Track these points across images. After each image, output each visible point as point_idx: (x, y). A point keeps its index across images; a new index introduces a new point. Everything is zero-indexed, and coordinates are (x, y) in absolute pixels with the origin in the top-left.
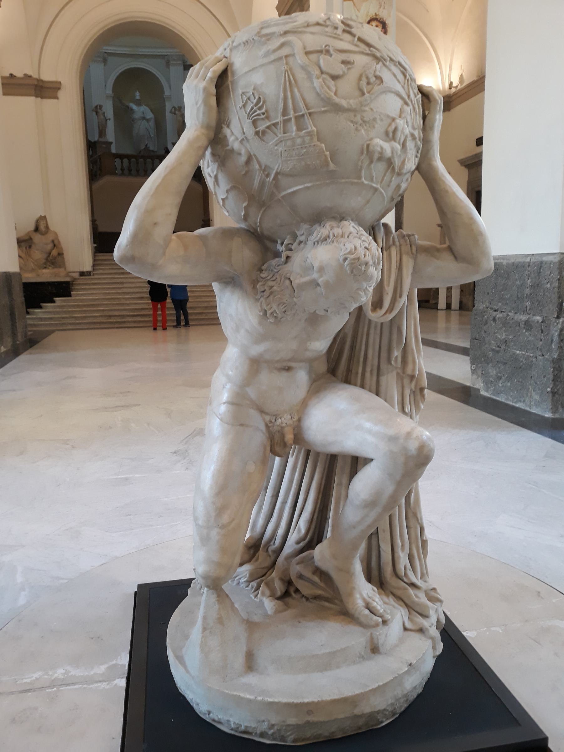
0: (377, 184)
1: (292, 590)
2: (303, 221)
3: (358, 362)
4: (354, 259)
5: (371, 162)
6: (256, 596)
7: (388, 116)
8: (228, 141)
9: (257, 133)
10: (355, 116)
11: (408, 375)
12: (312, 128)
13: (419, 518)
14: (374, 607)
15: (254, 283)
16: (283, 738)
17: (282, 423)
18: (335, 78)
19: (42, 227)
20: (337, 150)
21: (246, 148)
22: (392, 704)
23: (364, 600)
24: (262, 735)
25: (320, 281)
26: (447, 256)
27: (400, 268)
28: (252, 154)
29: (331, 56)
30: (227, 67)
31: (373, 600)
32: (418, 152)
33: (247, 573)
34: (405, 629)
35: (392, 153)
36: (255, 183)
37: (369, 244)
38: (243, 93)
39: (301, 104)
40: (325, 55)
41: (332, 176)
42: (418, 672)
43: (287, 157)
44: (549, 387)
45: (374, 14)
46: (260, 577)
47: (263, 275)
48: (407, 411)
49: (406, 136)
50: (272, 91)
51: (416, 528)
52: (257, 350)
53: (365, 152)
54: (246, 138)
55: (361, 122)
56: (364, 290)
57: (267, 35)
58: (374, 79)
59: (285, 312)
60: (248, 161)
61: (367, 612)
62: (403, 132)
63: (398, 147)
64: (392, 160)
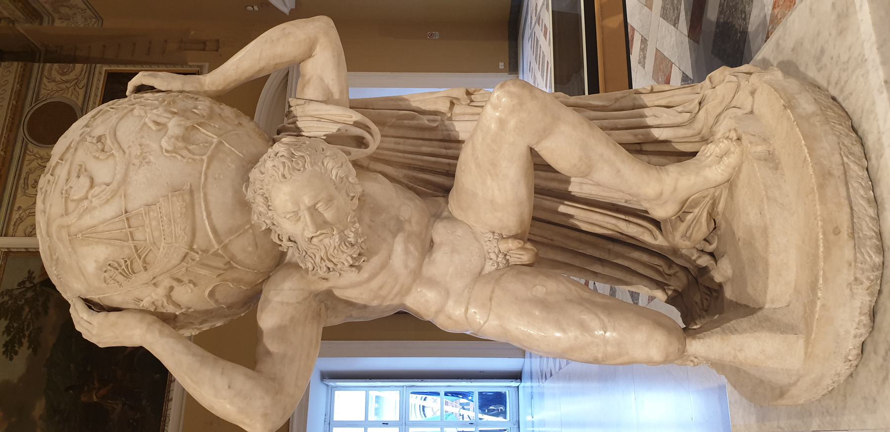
10: (134, 165)
18: (92, 185)
29: (71, 187)
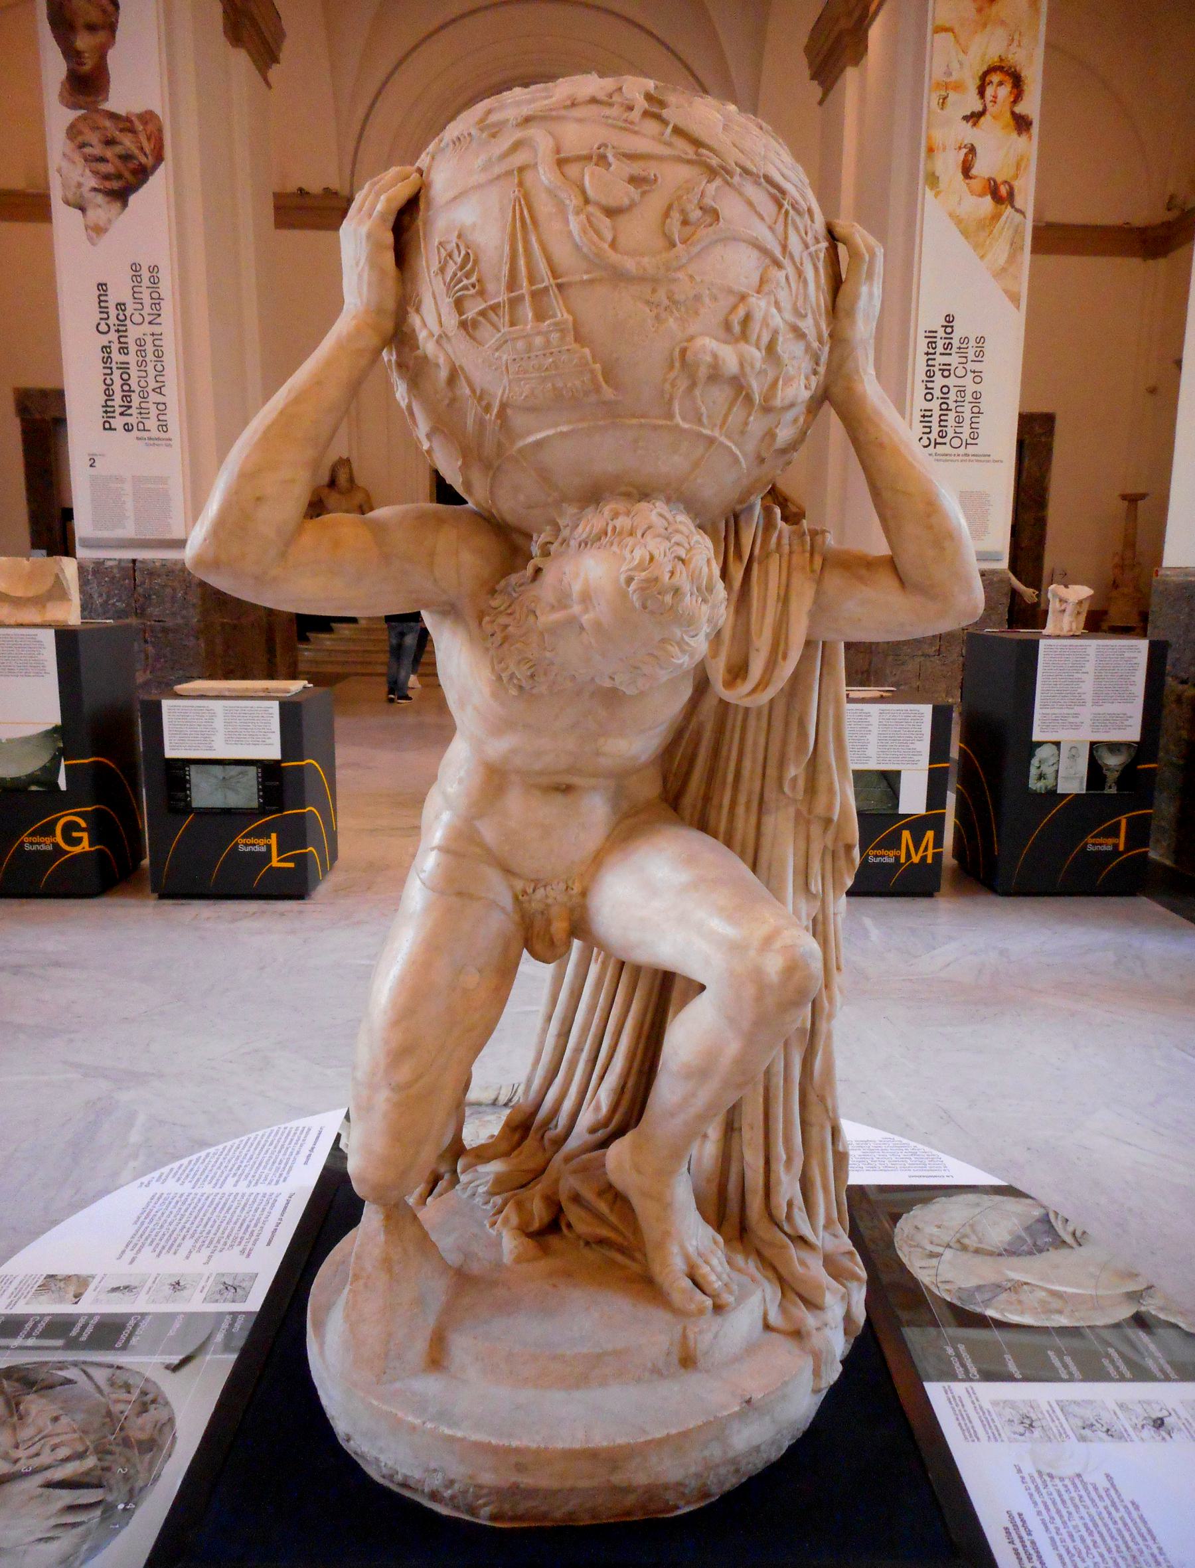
0: (712, 430)
3: (724, 783)
4: (647, 580)
5: (693, 384)
6: (493, 1224)
7: (730, 291)
8: (417, 339)
9: (463, 325)
10: (654, 291)
11: (820, 818)
12: (561, 314)
13: (830, 1107)
14: (704, 1276)
16: (472, 1510)
17: (547, 897)
18: (611, 212)
19: (342, 478)
20: (618, 359)
21: (447, 354)
22: (698, 1475)
23: (687, 1258)
24: (434, 1496)
25: (586, 619)
26: (886, 580)
27: (785, 600)
30: (419, 192)
31: (707, 1262)
32: (817, 364)
33: (491, 1177)
34: (767, 1327)
35: (742, 365)
37: (688, 551)
38: (440, 243)
39: (543, 267)
40: (596, 165)
41: (612, 413)
42: (767, 1418)
43: (518, 373)
45: (996, 59)
46: (511, 1188)
47: (494, 603)
48: (813, 889)
49: (776, 333)
51: (822, 1127)
52: (498, 747)
53: (677, 364)
55: (666, 302)
56: (678, 644)
57: (494, 125)
58: (699, 213)
59: (532, 676)
60: (452, 380)
62: (765, 322)
63: (756, 355)
64: (742, 380)
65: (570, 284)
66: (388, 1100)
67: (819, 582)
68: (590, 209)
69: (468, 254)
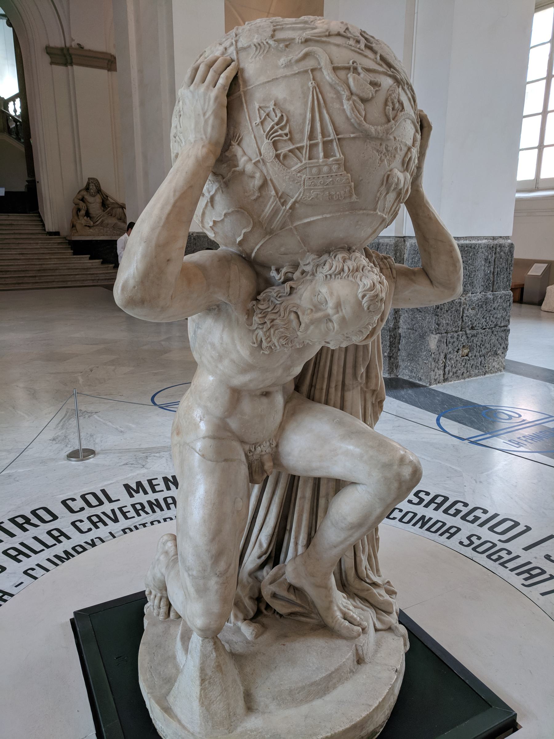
1: (263, 608)
2: (311, 251)
8: (237, 160)
9: (278, 156)
10: (381, 144)
14: (352, 617)
15: (250, 313)
17: (262, 451)
18: (364, 101)
28: (268, 178)
30: (237, 74)
36: (266, 210)
44: (386, 352)
50: (299, 109)
54: (263, 160)
61: (347, 623)
65: (343, 139)
66: (217, 583)
67: (396, 282)
68: (354, 98)
69: (282, 115)
